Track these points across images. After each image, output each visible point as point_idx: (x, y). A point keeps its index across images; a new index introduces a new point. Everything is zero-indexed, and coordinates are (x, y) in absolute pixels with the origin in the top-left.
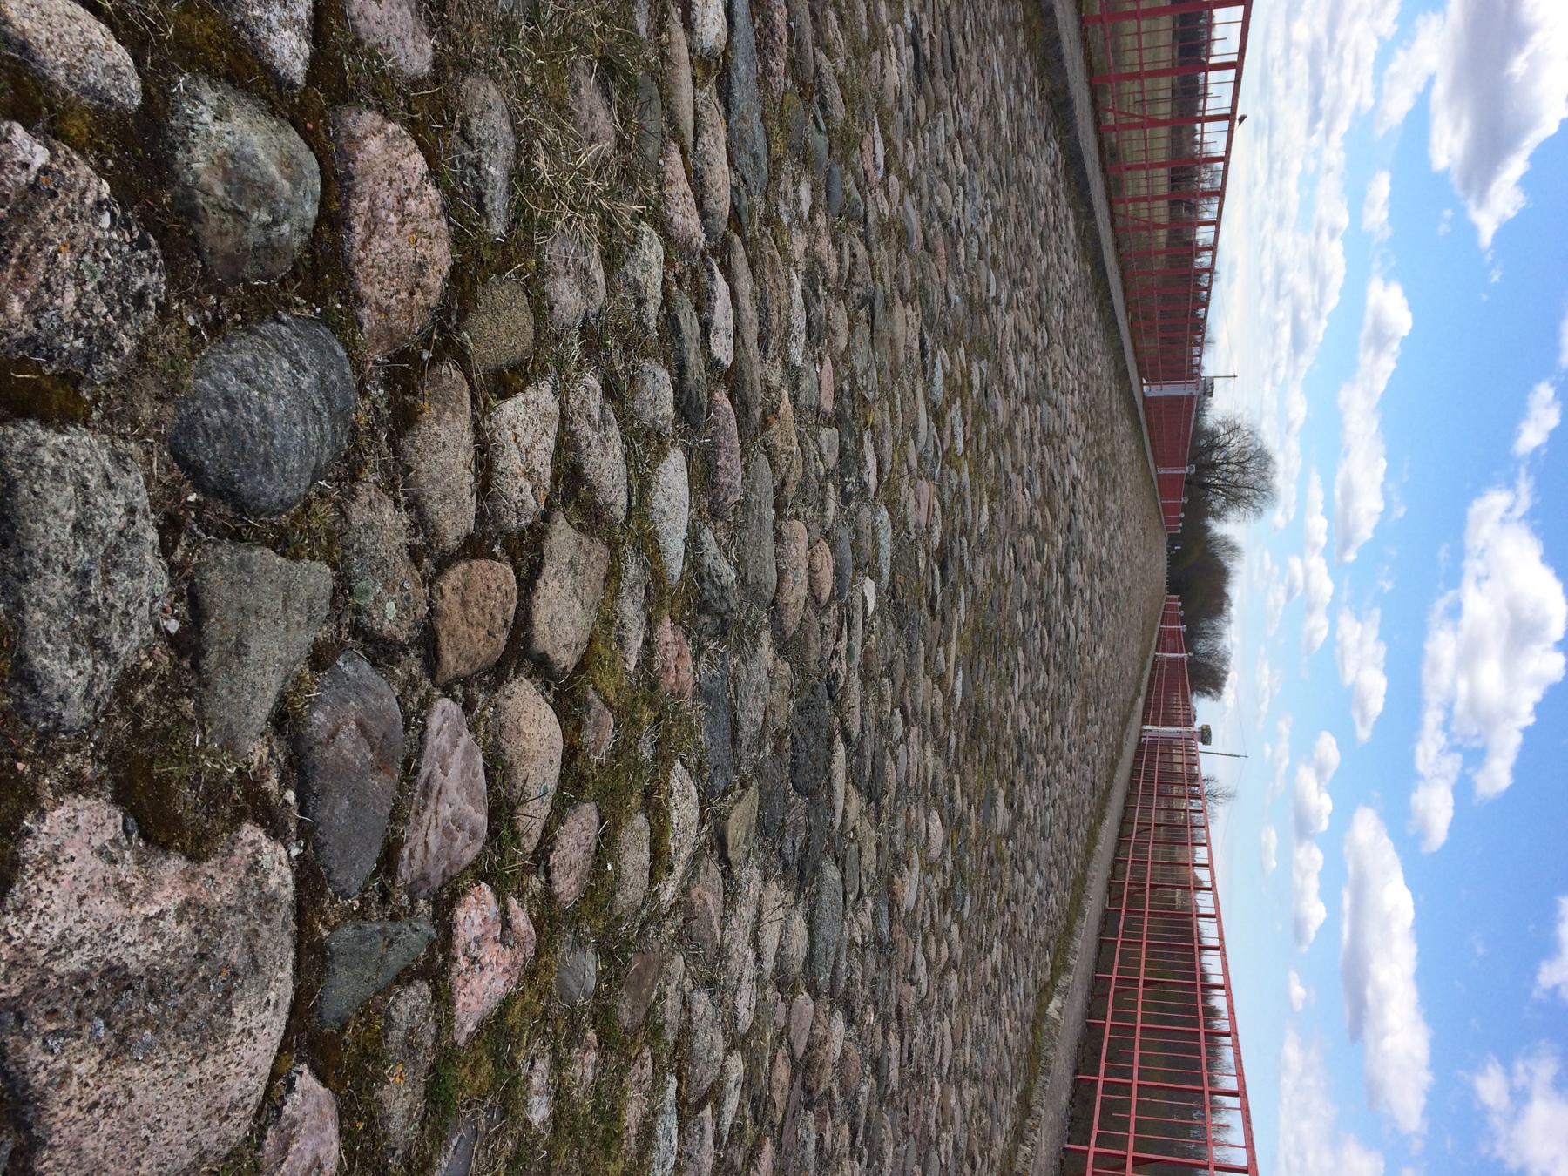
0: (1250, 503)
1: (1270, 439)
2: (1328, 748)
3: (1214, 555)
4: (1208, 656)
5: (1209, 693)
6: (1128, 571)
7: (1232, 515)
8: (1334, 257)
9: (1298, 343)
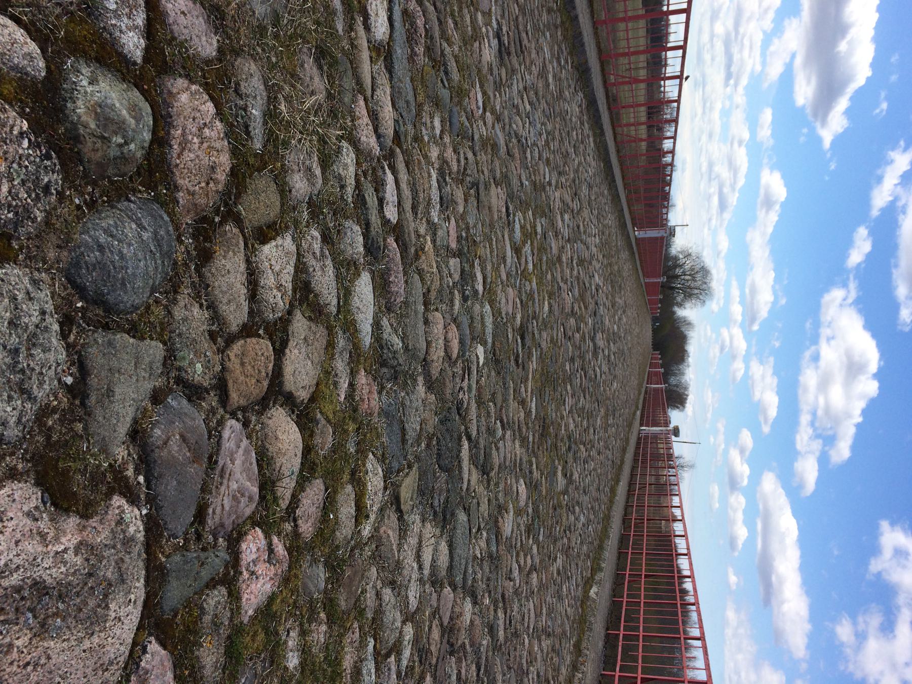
0: (698, 298)
1: (708, 260)
2: (746, 438)
3: (678, 328)
4: (677, 386)
5: (678, 408)
7: (688, 305)
8: (742, 157)
9: (723, 206)
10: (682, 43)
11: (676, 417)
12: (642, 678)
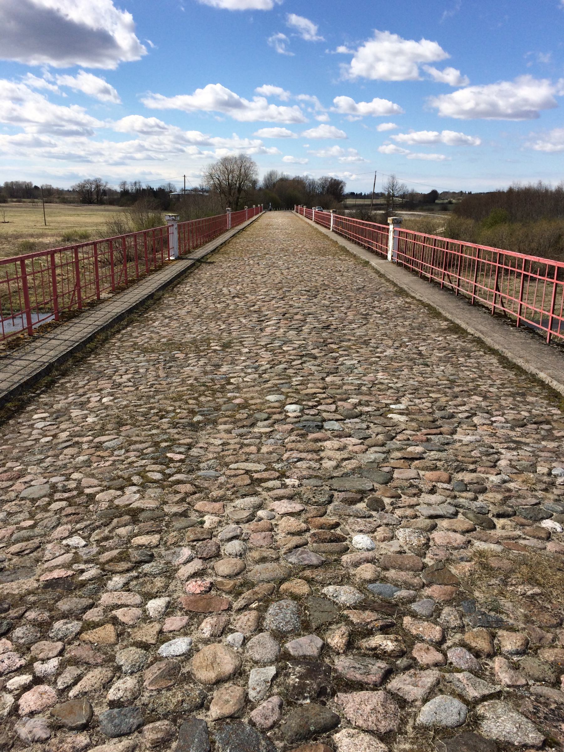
0: (248, 168)
3: (274, 184)
4: (323, 187)
5: (342, 187)
11: (347, 190)
12: (557, 280)
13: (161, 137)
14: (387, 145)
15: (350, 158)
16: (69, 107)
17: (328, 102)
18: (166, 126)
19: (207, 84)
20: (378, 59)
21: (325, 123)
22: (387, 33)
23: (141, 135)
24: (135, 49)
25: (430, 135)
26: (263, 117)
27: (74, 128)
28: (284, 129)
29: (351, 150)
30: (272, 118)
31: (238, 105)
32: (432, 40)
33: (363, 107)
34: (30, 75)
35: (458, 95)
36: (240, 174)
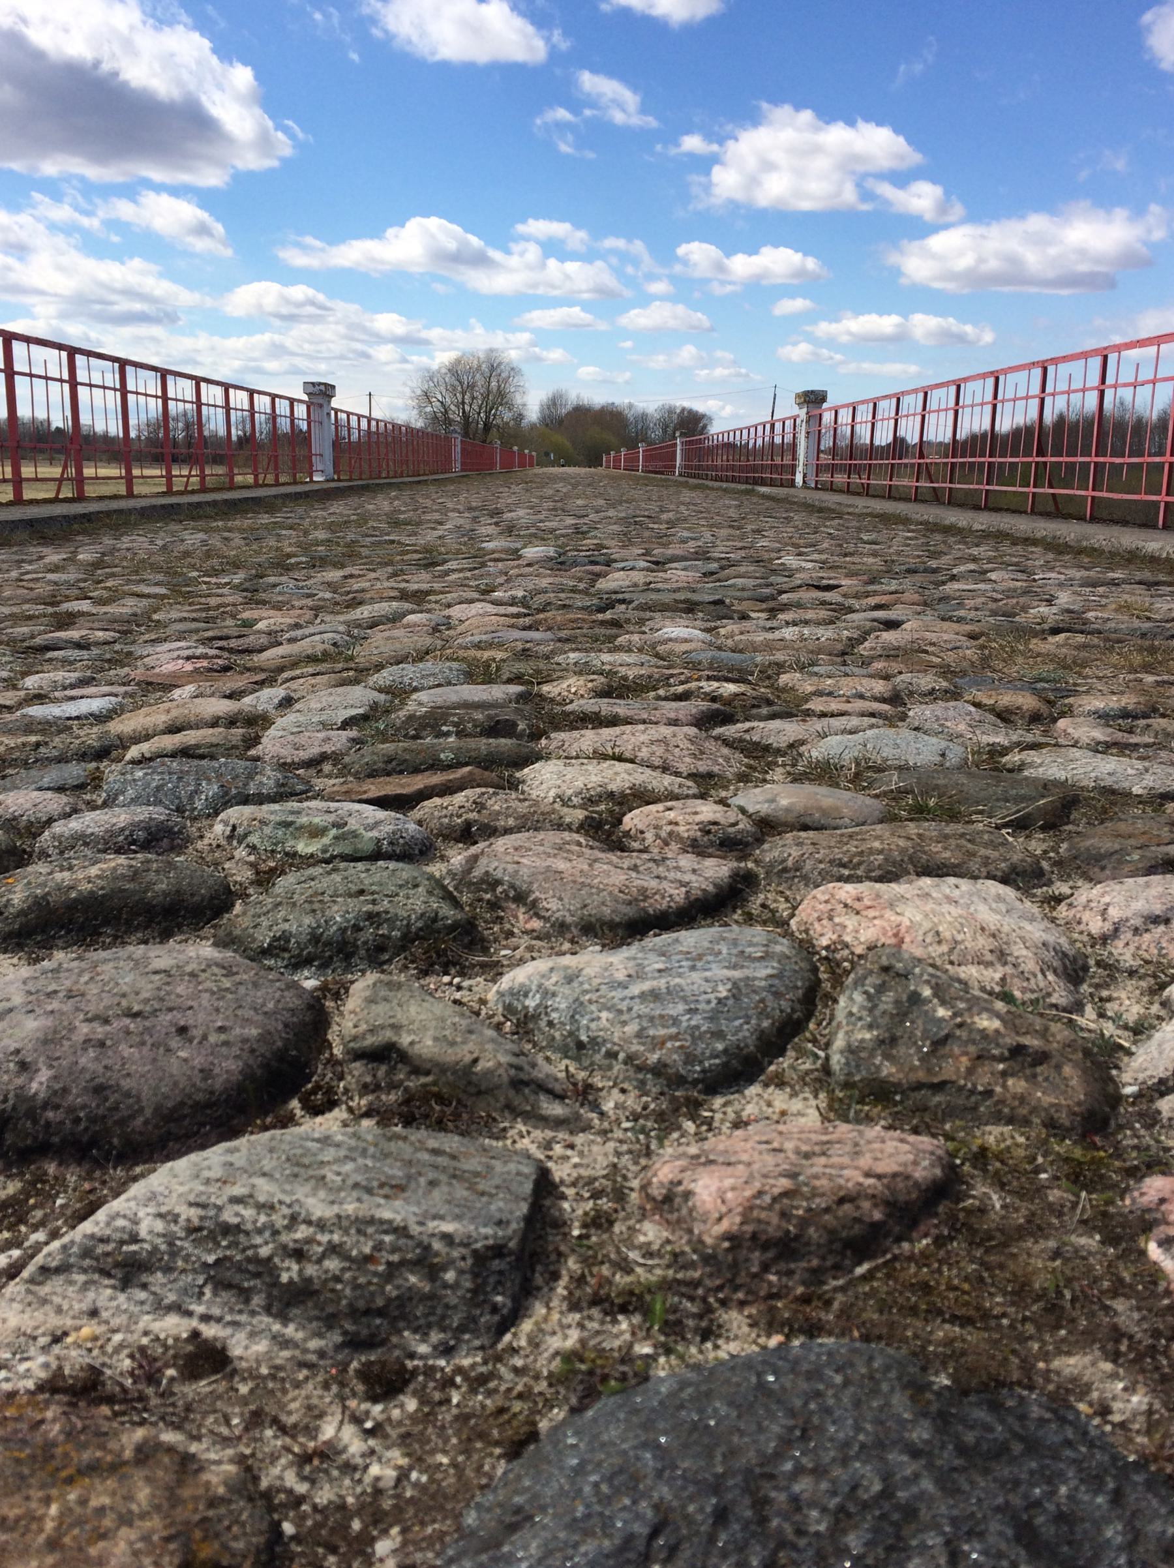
0: (506, 380)
5: (705, 427)
6: (580, 502)
7: (518, 400)
10: (64, 354)
11: (715, 429)
13: (318, 329)
14: (795, 344)
15: (719, 372)
16: (123, 263)
17: (665, 253)
18: (329, 304)
19: (408, 219)
20: (768, 166)
21: (663, 298)
22: (787, 109)
23: (277, 323)
24: (264, 143)
25: (887, 323)
26: (535, 285)
27: (138, 306)
28: (577, 309)
29: (719, 354)
30: (553, 287)
31: (480, 260)
32: (880, 124)
33: (741, 265)
34: (37, 196)
35: (938, 242)
36: (489, 392)
